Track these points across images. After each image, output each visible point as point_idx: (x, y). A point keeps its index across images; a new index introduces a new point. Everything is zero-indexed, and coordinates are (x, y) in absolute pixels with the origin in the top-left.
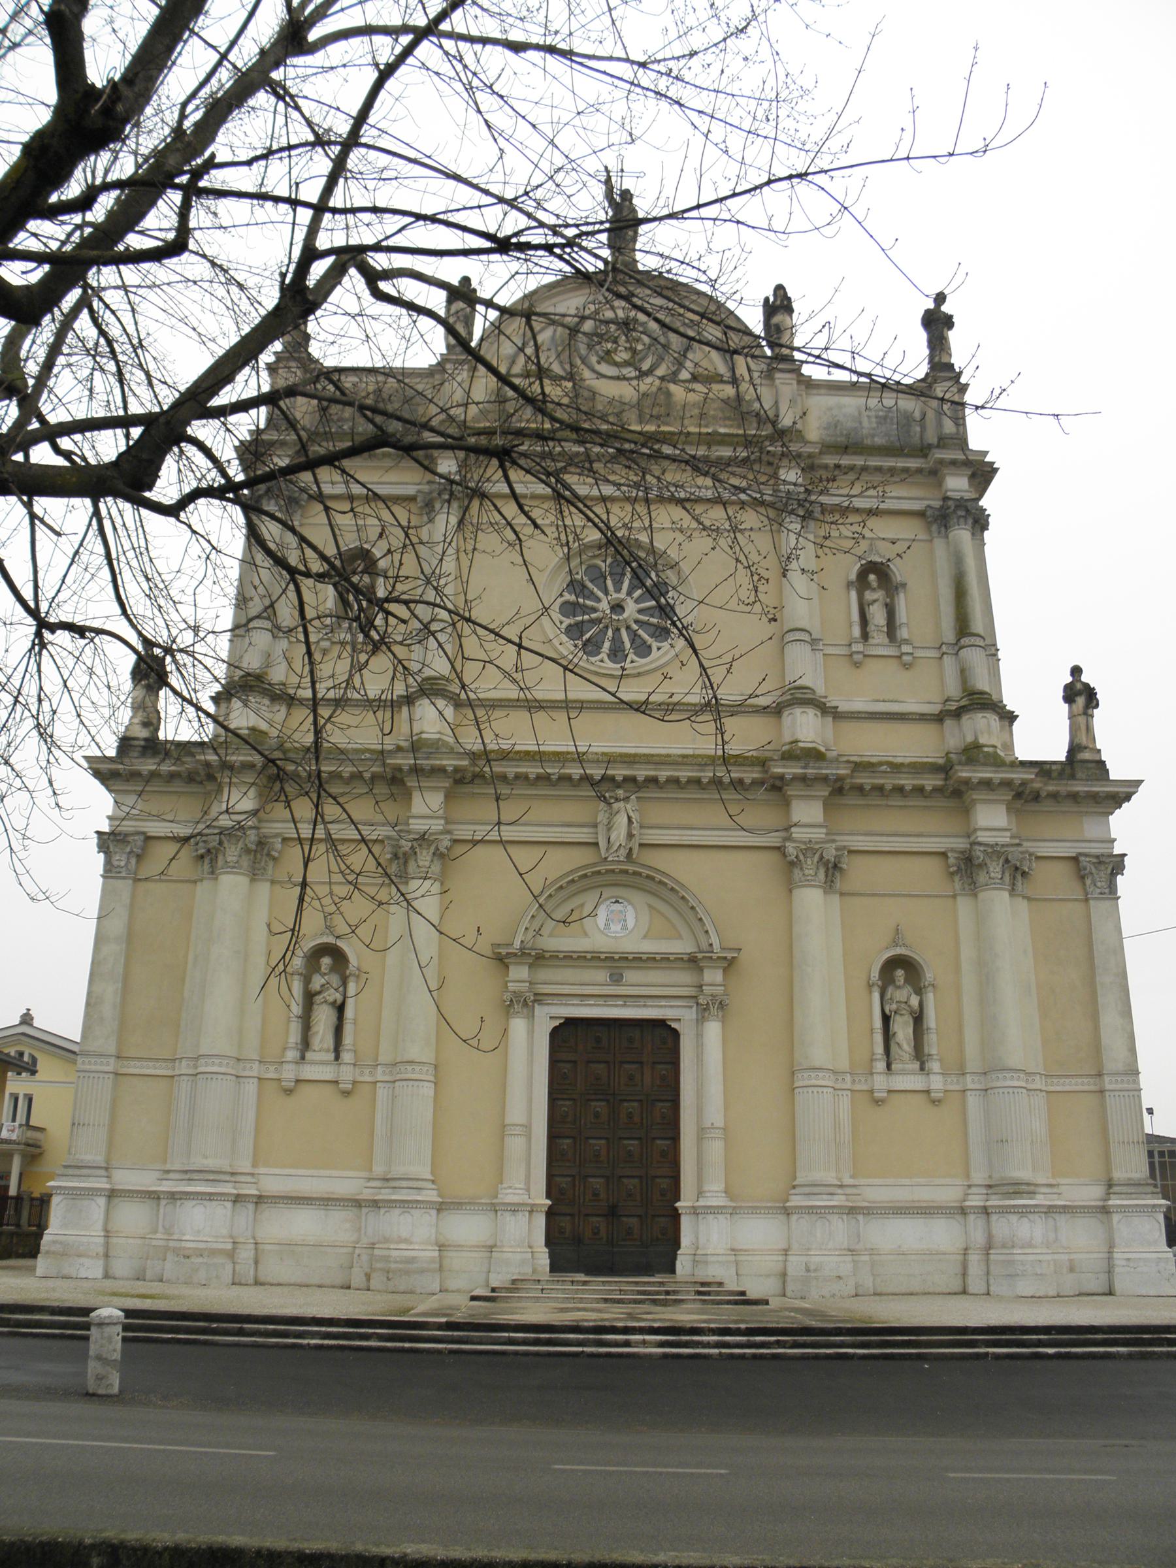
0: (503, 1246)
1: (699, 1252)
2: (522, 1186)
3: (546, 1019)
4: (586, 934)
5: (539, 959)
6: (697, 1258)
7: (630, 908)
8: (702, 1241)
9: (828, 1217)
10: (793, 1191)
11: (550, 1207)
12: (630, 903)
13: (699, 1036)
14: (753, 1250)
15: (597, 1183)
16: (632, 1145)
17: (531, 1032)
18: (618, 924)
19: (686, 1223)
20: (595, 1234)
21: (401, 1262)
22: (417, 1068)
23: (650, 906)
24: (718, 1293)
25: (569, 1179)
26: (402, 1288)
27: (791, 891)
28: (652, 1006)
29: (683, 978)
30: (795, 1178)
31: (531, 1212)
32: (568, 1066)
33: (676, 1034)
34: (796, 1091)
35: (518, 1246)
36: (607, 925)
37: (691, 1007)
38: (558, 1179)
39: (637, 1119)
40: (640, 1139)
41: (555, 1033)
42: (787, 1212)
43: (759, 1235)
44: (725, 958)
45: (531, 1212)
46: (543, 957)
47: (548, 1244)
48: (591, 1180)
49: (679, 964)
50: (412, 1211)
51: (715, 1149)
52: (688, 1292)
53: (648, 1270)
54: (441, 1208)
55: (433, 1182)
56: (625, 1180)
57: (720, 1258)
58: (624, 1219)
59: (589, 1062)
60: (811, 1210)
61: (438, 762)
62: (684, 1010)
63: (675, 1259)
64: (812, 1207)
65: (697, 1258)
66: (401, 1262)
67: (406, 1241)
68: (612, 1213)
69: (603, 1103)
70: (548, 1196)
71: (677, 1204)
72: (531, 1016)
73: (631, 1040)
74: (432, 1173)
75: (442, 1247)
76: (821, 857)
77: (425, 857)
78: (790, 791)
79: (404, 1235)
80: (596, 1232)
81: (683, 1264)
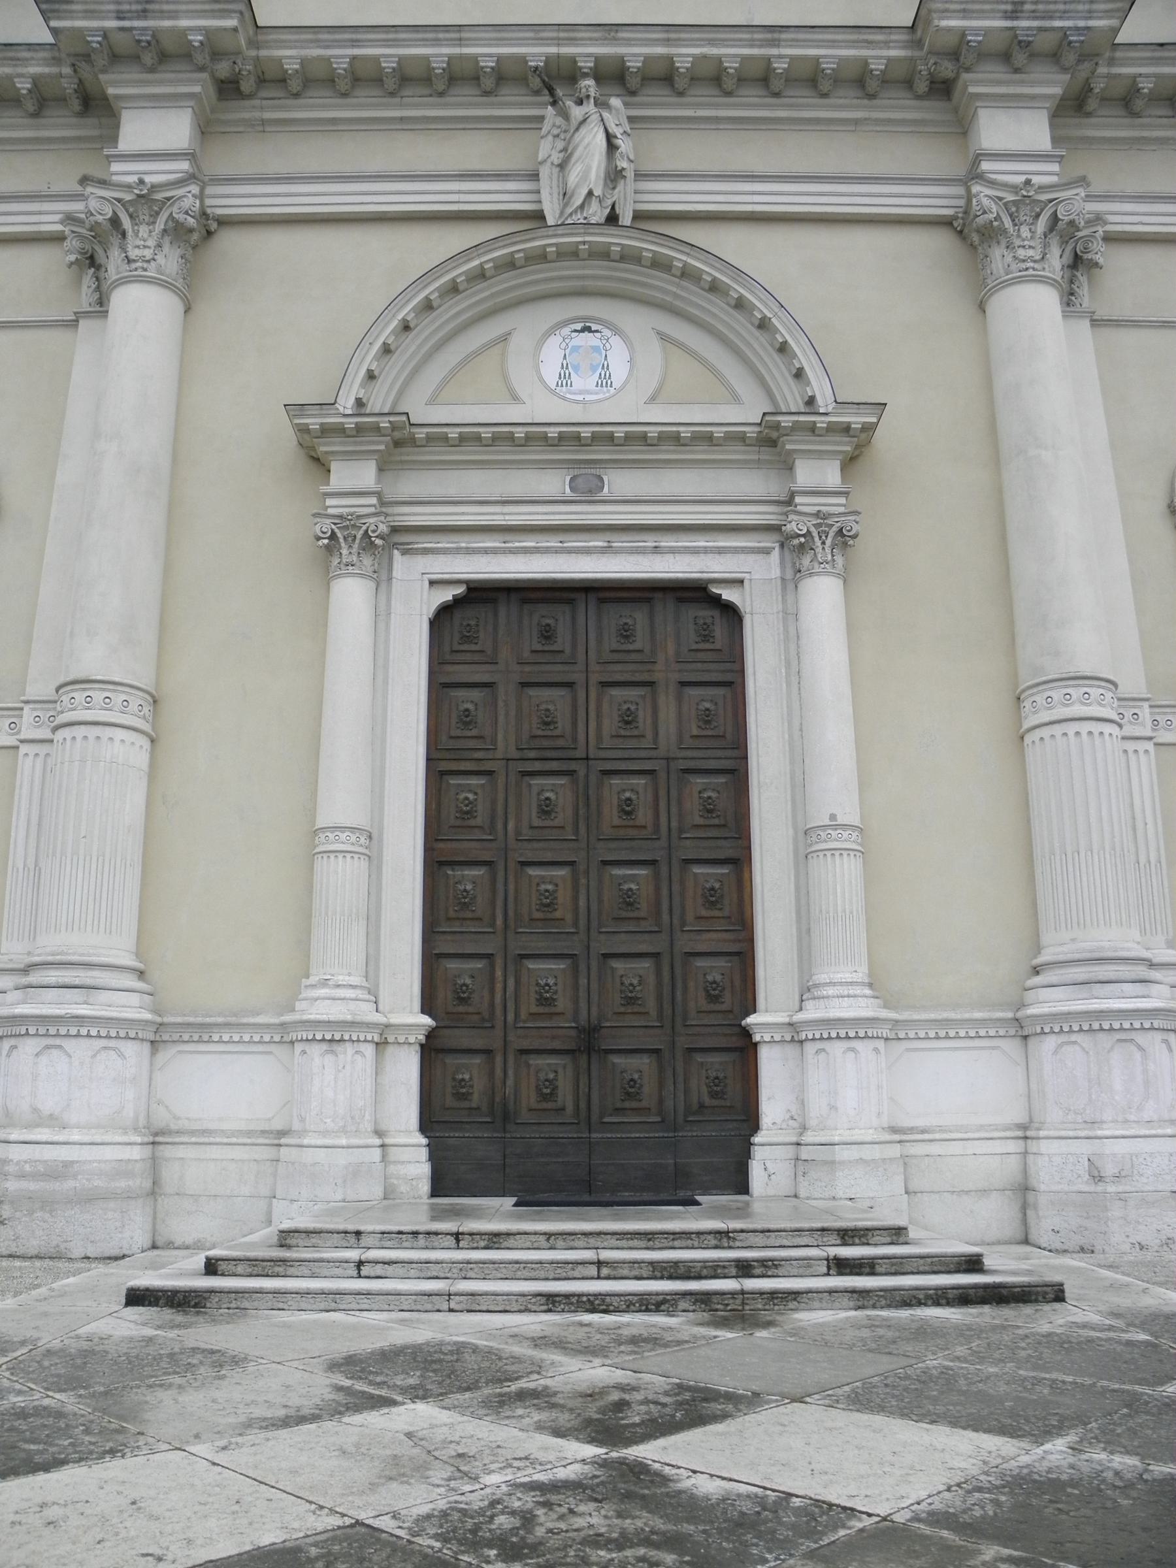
0: (303, 1133)
1: (809, 1137)
2: (356, 980)
3: (416, 590)
4: (515, 398)
5: (401, 444)
6: (805, 1153)
7: (616, 341)
8: (817, 1107)
9: (1140, 1038)
10: (1037, 980)
11: (431, 1035)
12: (616, 331)
13: (791, 616)
14: (942, 1129)
15: (548, 971)
16: (633, 878)
17: (381, 616)
18: (584, 368)
19: (773, 1067)
20: (545, 1098)
21: (35, 1176)
22: (98, 696)
23: (663, 337)
24: (898, 1266)
25: (479, 965)
26: (32, 1245)
27: (982, 307)
28: (673, 551)
29: (743, 487)
30: (1038, 949)
31: (381, 1045)
32: (476, 694)
33: (732, 613)
34: (1028, 739)
35: (344, 1130)
36: (564, 378)
37: (767, 551)
38: (453, 965)
39: (643, 816)
40: (653, 863)
41: (442, 618)
42: (1023, 1031)
43: (959, 1089)
44: (846, 429)
45: (381, 1045)
46: (412, 441)
47: (427, 1124)
48: (531, 965)
49: (736, 453)
50: (69, 1044)
51: (841, 879)
52: (805, 1266)
53: (676, 1190)
54: (159, 1036)
55: (141, 974)
56: (618, 965)
57: (868, 1153)
58: (616, 1059)
59: (524, 685)
60: (1094, 1024)
61: (167, 23)
62: (751, 558)
63: (747, 1155)
64: (1100, 1014)
65: (805, 1153)
66: (35, 1176)
67: (53, 1121)
68: (588, 1044)
69: (561, 781)
70: (426, 1008)
71: (751, 1020)
72: (382, 579)
73: (626, 633)
74: (138, 955)
75: (157, 1138)
76: (1055, 219)
77: (143, 240)
78: (976, 83)
79: (48, 1105)
80: (547, 1093)
81: (767, 1167)
